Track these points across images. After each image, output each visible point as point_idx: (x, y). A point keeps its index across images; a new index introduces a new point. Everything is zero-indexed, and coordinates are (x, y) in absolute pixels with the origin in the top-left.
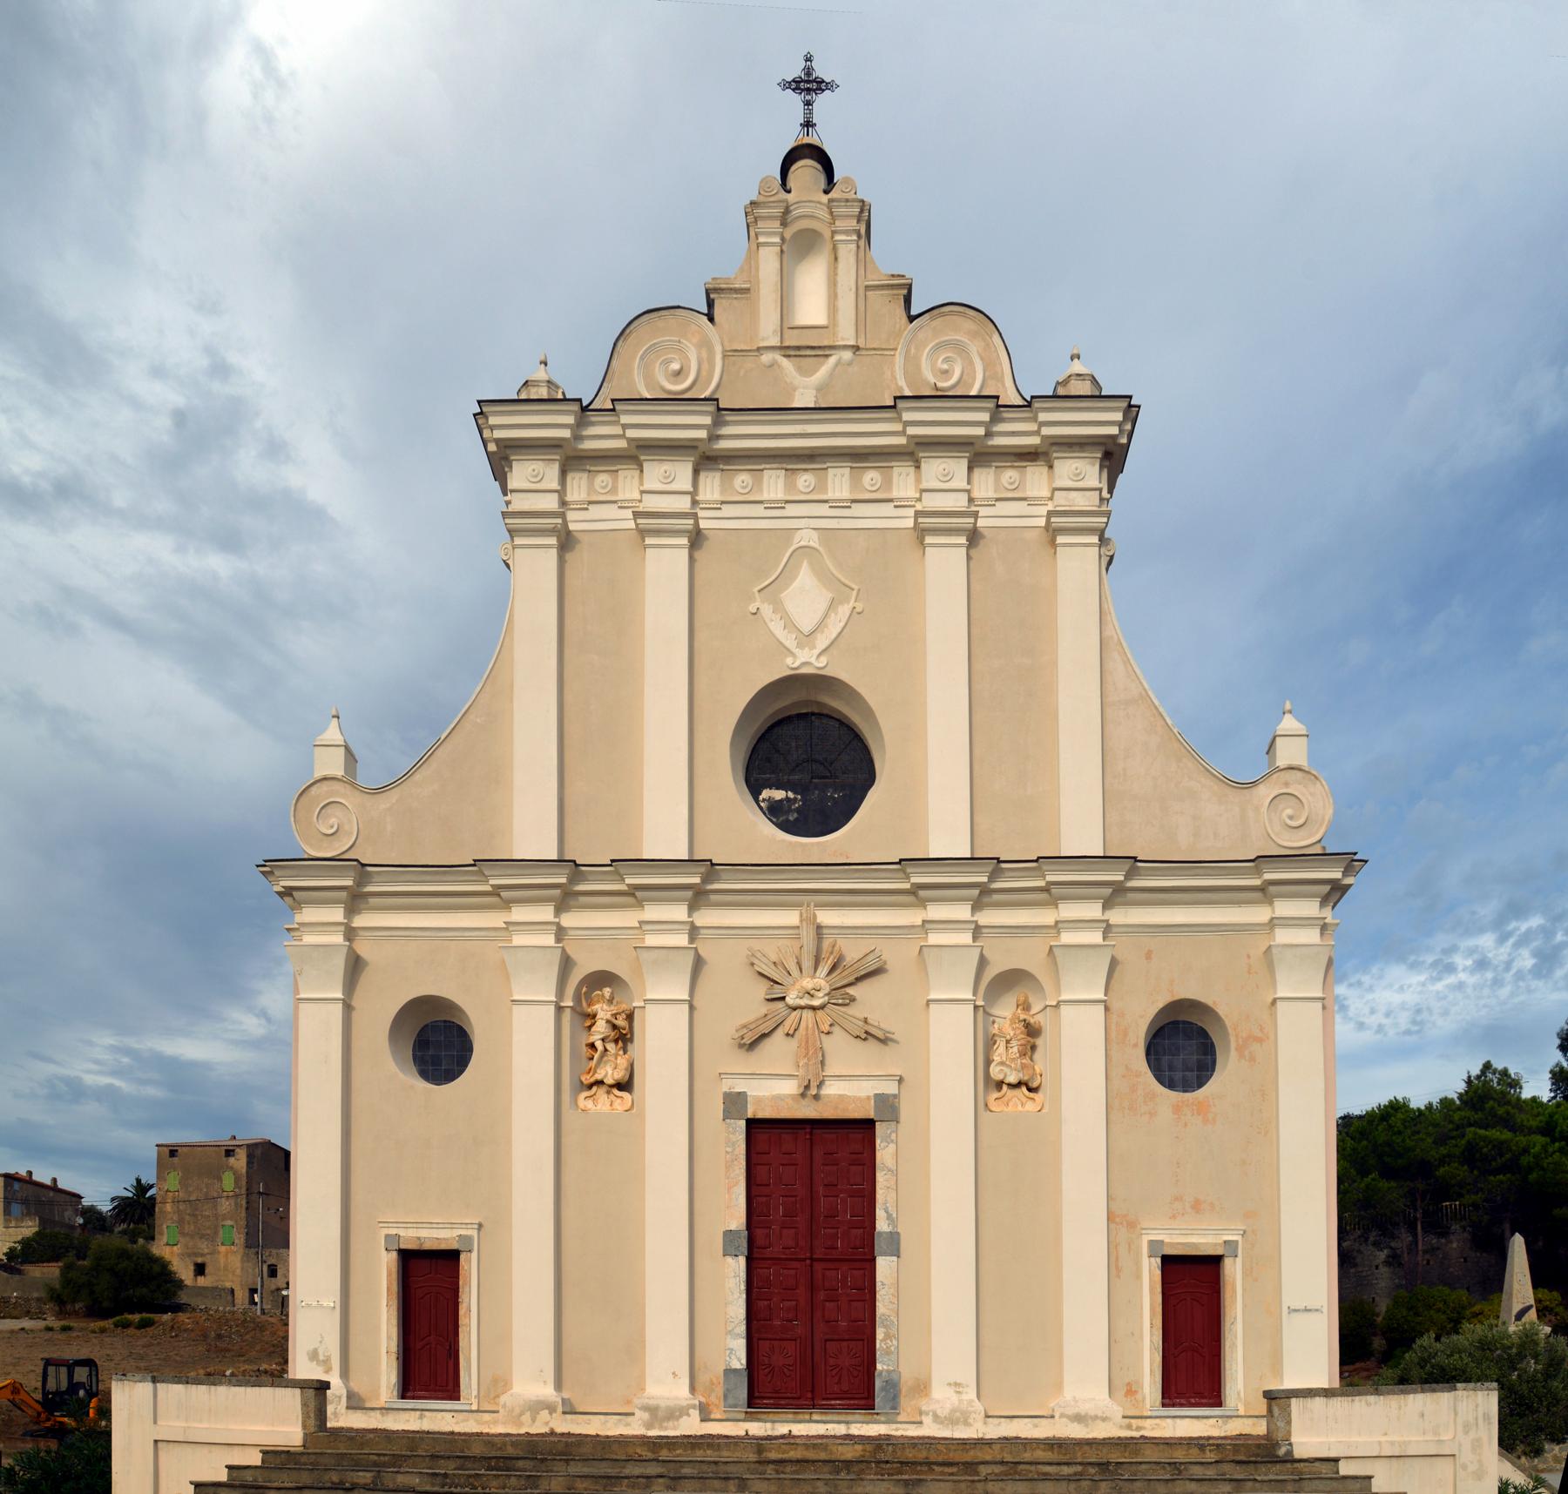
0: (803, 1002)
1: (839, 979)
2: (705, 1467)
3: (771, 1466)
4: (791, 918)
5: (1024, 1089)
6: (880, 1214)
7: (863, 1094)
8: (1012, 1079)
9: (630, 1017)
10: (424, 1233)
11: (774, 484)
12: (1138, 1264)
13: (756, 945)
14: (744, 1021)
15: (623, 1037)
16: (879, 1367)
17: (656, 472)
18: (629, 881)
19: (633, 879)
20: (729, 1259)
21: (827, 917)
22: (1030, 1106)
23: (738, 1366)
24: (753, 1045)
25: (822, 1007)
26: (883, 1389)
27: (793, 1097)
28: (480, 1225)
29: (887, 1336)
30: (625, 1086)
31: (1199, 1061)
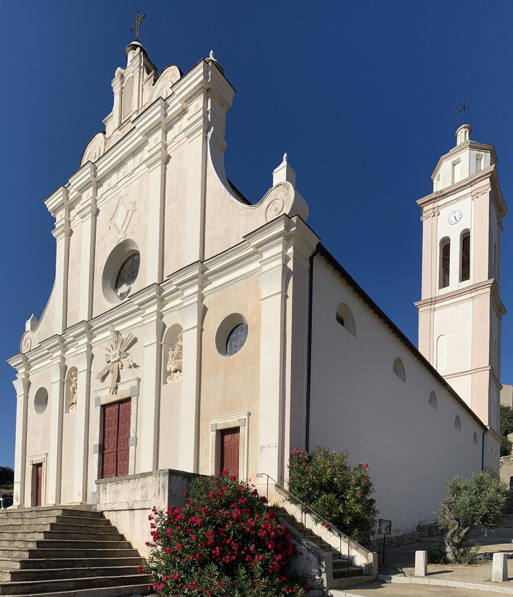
4: (108, 333)
11: (114, 178)
25: (119, 360)
28: (249, 414)
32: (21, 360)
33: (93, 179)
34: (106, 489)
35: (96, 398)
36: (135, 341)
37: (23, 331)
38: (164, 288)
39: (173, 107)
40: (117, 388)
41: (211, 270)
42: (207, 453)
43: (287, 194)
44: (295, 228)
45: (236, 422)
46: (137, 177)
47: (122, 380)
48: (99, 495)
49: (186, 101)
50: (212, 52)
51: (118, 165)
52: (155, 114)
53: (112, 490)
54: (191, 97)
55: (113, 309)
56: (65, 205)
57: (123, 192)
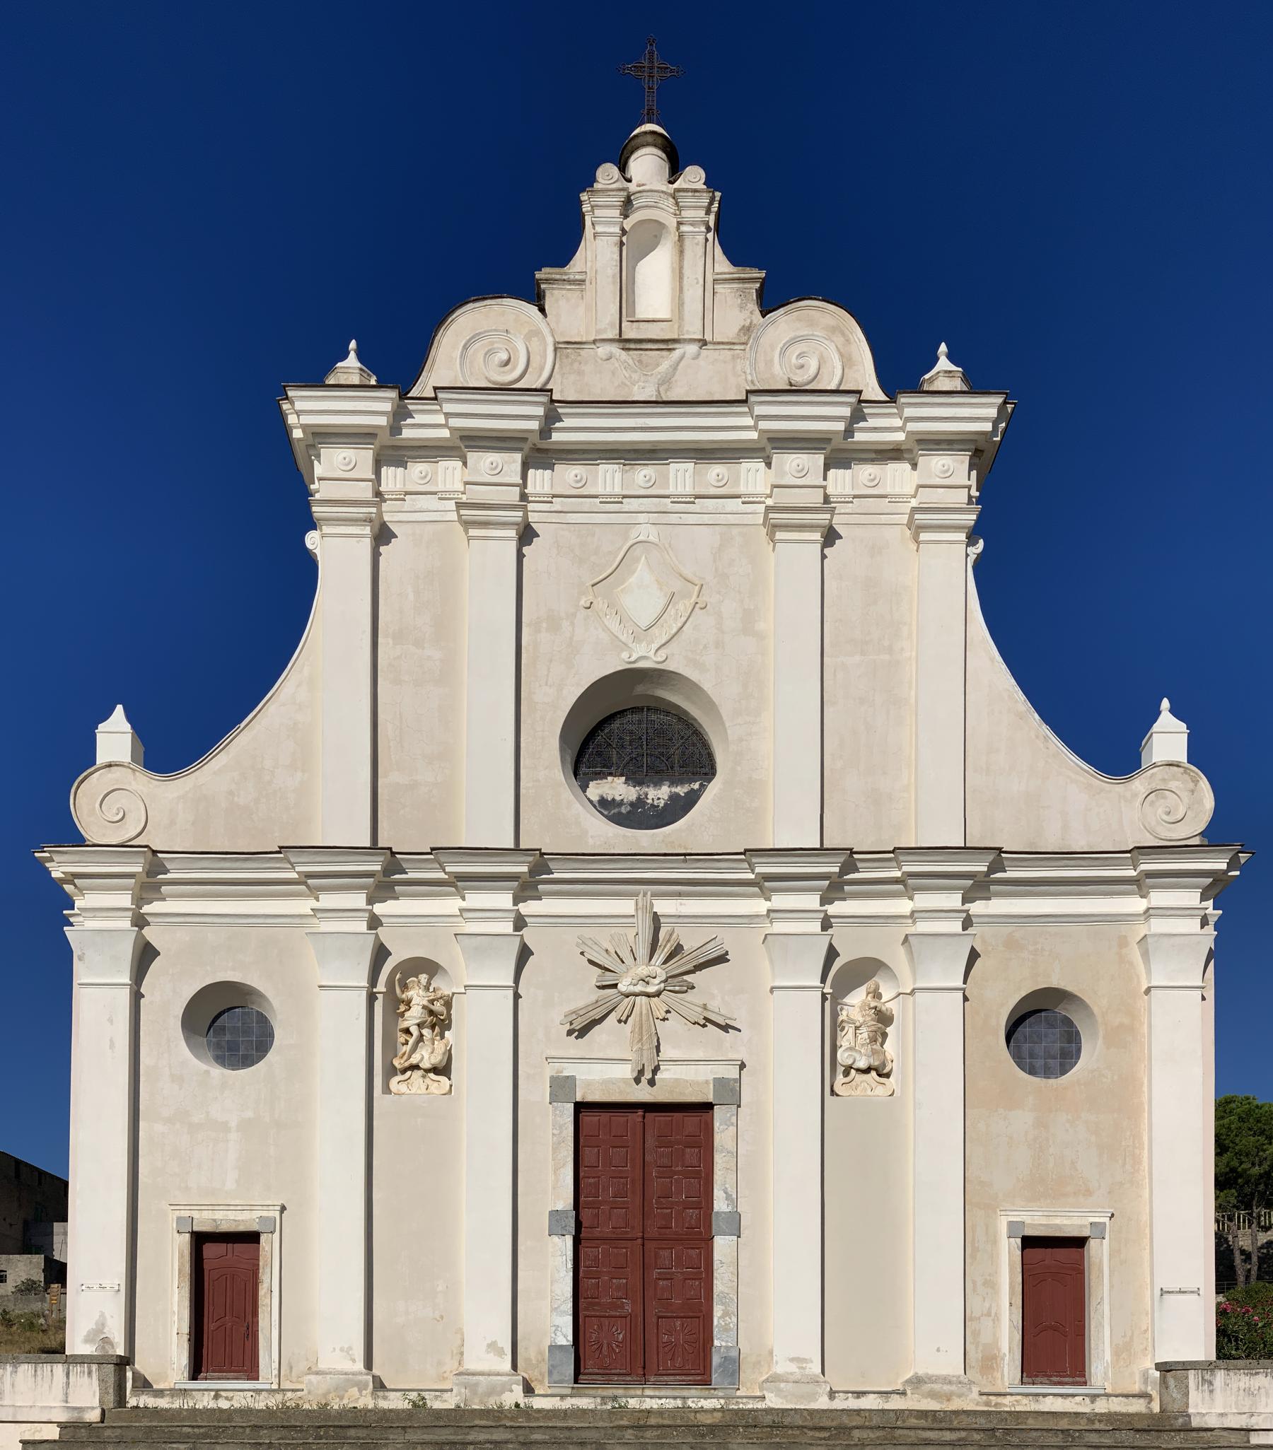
0: (639, 988)
1: (676, 966)
2: (557, 1433)
3: (630, 1431)
4: (625, 906)
5: (873, 1073)
6: (718, 1194)
7: (701, 1078)
8: (862, 1064)
9: (448, 1004)
10: (219, 1215)
11: (608, 477)
12: (995, 1242)
13: (587, 933)
14: (573, 1007)
15: (439, 1021)
16: (716, 1343)
17: (484, 462)
18: (758, 870)
19: (459, 867)
20: (555, 1238)
21: (663, 907)
22: (880, 1091)
23: (565, 1343)
24: (583, 1032)
25: (658, 994)
26: (720, 1366)
27: (624, 1080)
28: (283, 1208)
29: (726, 1314)
30: (443, 1070)
31: (1062, 1049)
32: (138, 869)
33: (535, 439)
34: (1211, 1383)
35: (552, 1078)
36: (722, 959)
37: (85, 757)
38: (859, 865)
39: (875, 429)
40: (656, 1070)
41: (1010, 874)
42: (991, 1284)
43: (1193, 791)
44: (1237, 873)
45: (1081, 1226)
46: (706, 519)
47: (667, 1052)
48: (1187, 1394)
49: (919, 441)
50: (943, 348)
51: (636, 451)
52: (523, 417)
53: (1235, 1386)
54: (938, 442)
55: (665, 855)
56: (377, 442)
57: (646, 532)
